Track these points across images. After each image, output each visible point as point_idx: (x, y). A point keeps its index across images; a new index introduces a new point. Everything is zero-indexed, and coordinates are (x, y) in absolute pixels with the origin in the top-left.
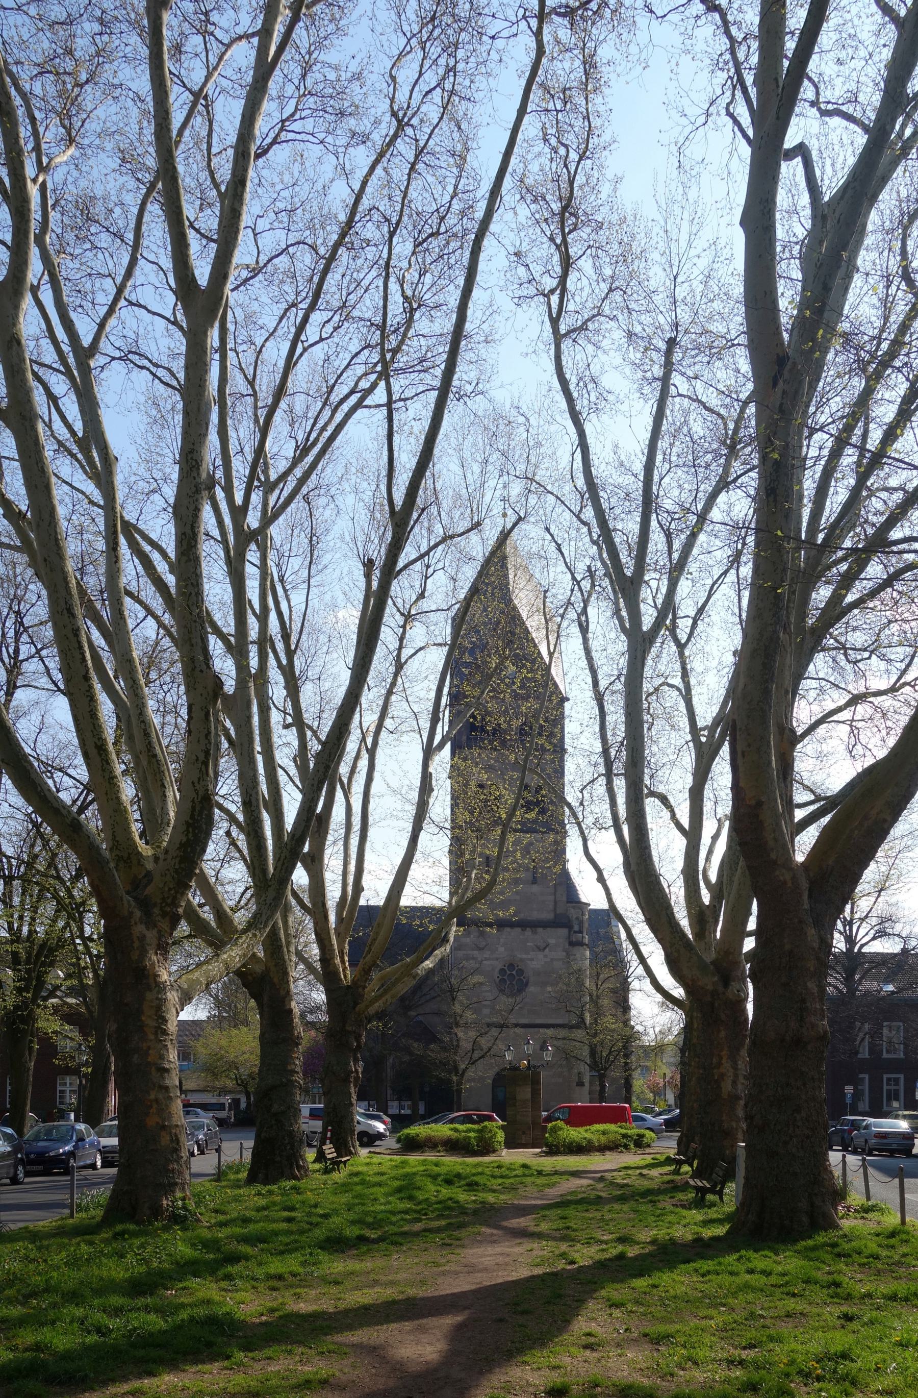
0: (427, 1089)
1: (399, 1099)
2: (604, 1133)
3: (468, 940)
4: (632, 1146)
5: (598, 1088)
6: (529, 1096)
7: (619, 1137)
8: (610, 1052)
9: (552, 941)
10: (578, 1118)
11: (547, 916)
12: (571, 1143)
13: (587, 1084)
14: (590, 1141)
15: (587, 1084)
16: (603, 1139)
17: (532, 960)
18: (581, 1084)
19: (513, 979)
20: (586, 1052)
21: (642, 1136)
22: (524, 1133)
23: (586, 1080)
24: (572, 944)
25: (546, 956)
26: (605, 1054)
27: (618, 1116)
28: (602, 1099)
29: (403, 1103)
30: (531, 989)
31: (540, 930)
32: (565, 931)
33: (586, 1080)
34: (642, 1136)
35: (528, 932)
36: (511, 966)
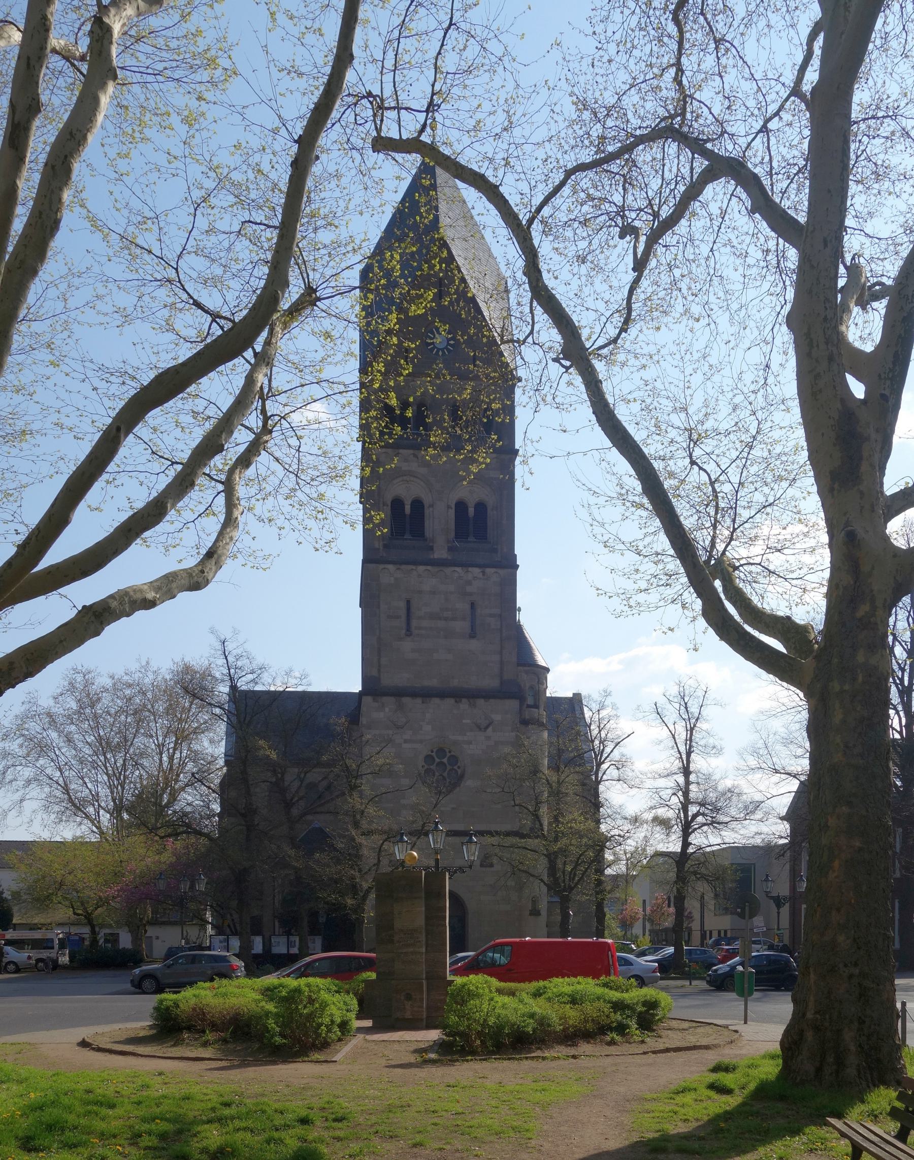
0: (322, 920)
1: (288, 934)
2: (574, 1000)
3: (382, 715)
4: (633, 1024)
5: (559, 918)
6: (421, 921)
7: (607, 1008)
8: (577, 864)
9: (497, 717)
10: (527, 965)
11: (490, 682)
12: (500, 1028)
13: (544, 913)
14: (543, 1022)
15: (544, 913)
16: (573, 1014)
17: (470, 743)
18: (535, 912)
19: (444, 769)
20: (542, 867)
21: (652, 1005)
22: (409, 997)
23: (543, 906)
24: (525, 722)
25: (488, 738)
26: (569, 868)
27: (595, 962)
28: (565, 933)
29: (292, 938)
30: (469, 783)
31: (481, 702)
32: (514, 704)
33: (543, 906)
34: (652, 1005)
35: (464, 705)
36: (441, 751)
